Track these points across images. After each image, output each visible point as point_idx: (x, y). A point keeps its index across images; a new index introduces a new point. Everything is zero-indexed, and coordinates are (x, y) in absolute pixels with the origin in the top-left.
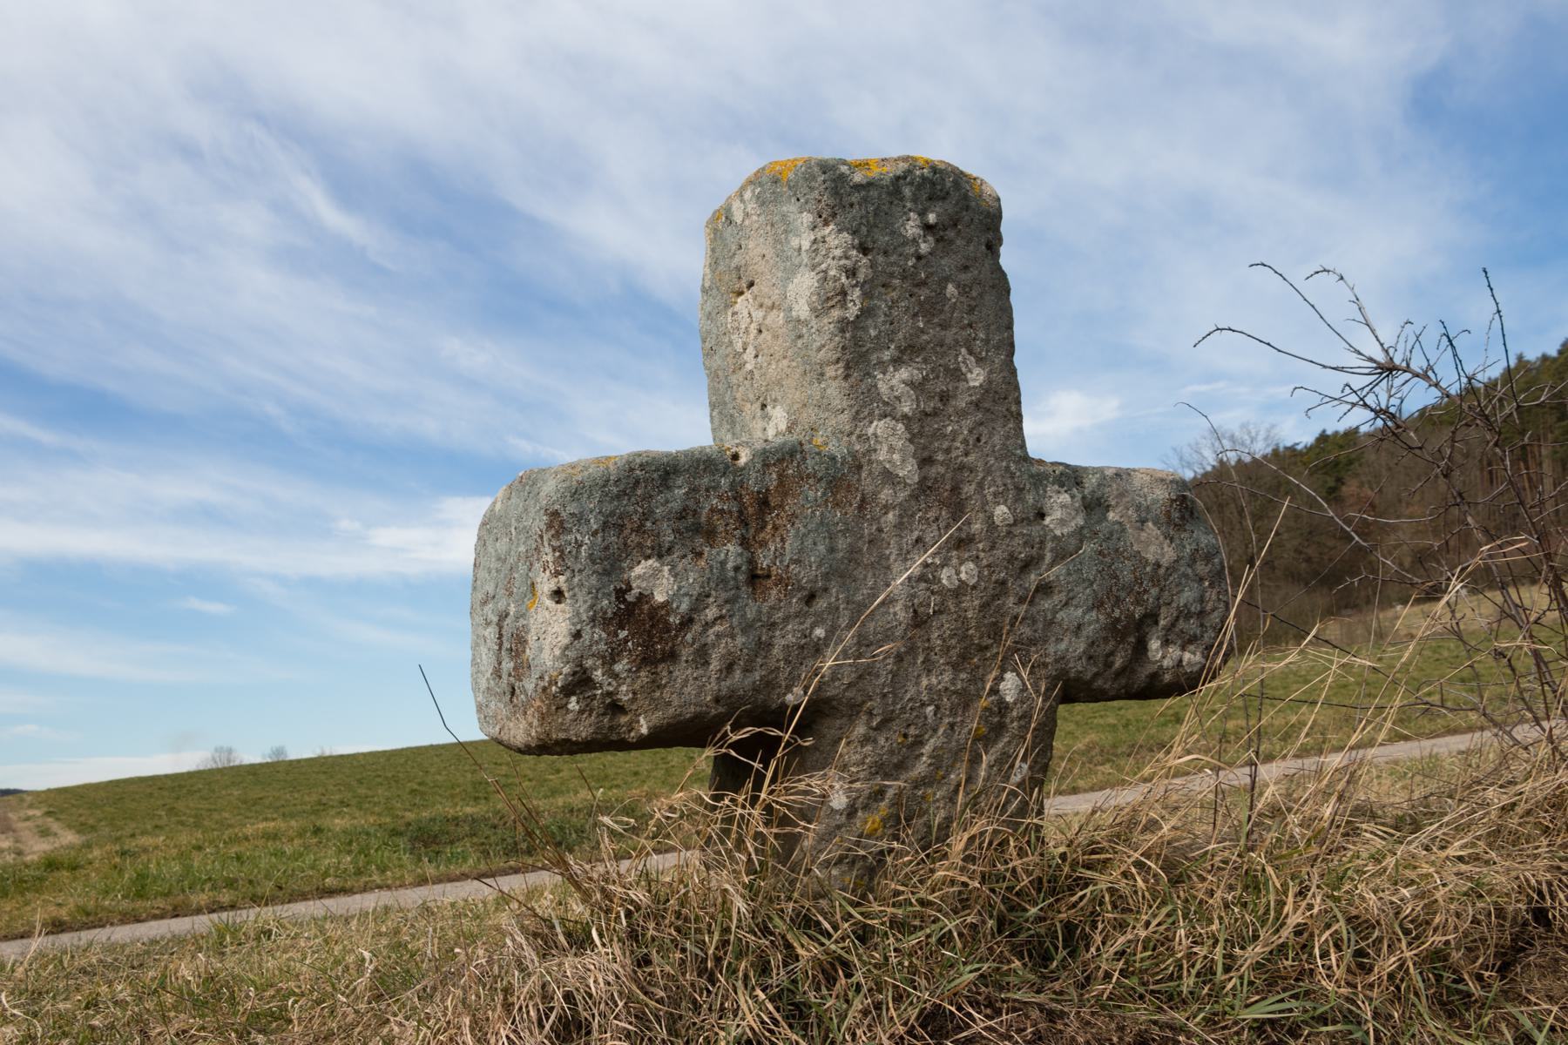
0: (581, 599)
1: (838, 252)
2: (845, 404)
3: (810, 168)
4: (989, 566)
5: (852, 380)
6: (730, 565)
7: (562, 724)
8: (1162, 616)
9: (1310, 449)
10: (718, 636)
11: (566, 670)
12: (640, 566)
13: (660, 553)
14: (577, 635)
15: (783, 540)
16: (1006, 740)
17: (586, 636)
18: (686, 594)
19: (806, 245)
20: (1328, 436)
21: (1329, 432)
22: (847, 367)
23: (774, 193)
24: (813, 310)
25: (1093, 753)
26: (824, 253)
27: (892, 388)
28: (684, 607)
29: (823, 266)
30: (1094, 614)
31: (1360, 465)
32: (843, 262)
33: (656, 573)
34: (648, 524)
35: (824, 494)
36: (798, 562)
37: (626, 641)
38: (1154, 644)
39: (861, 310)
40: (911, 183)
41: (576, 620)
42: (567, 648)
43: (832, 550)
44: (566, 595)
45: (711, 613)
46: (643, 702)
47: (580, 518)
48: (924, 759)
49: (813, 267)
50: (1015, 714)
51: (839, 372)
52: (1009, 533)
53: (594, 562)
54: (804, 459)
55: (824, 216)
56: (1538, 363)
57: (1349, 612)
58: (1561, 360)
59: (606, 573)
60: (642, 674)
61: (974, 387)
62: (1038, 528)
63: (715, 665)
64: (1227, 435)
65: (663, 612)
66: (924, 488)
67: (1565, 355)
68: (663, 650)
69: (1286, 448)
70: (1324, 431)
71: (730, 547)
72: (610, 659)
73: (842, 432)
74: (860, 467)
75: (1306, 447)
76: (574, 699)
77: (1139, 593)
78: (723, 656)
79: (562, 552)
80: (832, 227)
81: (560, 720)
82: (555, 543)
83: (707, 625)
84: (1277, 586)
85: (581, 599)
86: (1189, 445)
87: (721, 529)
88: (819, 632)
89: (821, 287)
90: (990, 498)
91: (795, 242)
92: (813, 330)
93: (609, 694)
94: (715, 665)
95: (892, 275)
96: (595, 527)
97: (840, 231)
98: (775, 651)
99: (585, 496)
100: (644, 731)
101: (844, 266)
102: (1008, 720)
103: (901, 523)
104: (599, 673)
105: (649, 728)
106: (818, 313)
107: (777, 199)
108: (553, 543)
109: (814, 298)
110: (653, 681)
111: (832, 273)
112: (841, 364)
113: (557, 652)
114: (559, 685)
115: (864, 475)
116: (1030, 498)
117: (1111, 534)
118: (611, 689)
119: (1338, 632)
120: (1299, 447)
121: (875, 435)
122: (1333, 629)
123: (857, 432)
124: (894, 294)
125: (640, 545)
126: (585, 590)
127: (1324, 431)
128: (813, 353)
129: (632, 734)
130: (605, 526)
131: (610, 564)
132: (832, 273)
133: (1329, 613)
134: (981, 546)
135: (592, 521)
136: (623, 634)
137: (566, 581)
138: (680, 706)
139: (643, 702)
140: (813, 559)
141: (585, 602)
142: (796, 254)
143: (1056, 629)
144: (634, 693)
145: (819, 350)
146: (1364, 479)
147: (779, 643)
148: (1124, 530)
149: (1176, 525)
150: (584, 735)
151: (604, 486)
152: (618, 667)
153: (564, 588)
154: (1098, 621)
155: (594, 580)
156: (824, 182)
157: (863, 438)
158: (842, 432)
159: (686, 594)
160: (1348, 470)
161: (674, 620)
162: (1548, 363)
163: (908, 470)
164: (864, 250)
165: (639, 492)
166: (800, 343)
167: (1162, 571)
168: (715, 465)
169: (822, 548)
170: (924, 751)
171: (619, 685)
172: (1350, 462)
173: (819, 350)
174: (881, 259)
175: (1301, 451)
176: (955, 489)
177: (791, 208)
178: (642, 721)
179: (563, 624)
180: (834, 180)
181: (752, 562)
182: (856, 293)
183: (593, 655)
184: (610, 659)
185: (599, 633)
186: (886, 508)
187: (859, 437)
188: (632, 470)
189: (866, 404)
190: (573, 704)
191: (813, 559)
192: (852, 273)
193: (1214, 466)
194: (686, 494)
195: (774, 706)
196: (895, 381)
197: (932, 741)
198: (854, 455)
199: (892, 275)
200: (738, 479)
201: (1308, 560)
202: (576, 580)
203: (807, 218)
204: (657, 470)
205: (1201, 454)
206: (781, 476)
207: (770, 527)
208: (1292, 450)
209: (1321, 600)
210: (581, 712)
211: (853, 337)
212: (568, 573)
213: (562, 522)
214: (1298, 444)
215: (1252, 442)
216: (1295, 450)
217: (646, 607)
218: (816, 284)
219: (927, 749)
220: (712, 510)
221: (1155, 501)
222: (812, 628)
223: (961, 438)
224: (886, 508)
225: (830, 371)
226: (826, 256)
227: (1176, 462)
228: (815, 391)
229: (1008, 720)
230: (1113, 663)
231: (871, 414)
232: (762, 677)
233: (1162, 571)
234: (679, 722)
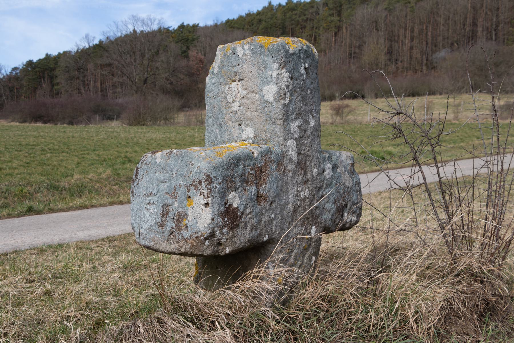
0: (215, 207)
1: (285, 80)
2: (282, 134)
3: (279, 46)
4: (311, 190)
5: (284, 126)
6: (253, 193)
7: (202, 249)
8: (348, 205)
9: (175, 31)
10: (250, 219)
11: (209, 232)
12: (231, 195)
13: (236, 189)
14: (213, 219)
15: (266, 184)
16: (311, 249)
17: (216, 220)
18: (242, 204)
19: (275, 75)
20: (184, 26)
21: (185, 24)
22: (284, 121)
23: (260, 51)
24: (275, 99)
25: (110, 180)
26: (281, 79)
27: (294, 128)
28: (242, 209)
29: (280, 84)
30: (334, 205)
31: (198, 42)
32: (287, 83)
33: (234, 198)
34: (233, 179)
35: (276, 167)
36: (269, 191)
37: (227, 221)
38: (346, 214)
39: (289, 101)
40: (302, 52)
41: (213, 214)
42: (210, 224)
43: (277, 187)
44: (210, 205)
45: (248, 211)
46: (229, 242)
47: (216, 177)
48: (293, 257)
49: (277, 84)
50: (314, 240)
51: (281, 123)
52: (316, 178)
53: (220, 194)
54: (271, 154)
55: (282, 65)
56: (277, 7)
57: (187, 109)
58: (286, 7)
59: (222, 197)
60: (230, 233)
61: (312, 127)
62: (323, 176)
63: (249, 229)
64: (141, 19)
65: (236, 211)
66: (298, 163)
67: (288, 5)
68: (236, 224)
69: (164, 28)
70: (183, 23)
71: (253, 187)
72: (221, 228)
73: (279, 144)
74: (284, 157)
75: (174, 29)
76: (207, 241)
77: (344, 197)
78: (251, 226)
79: (211, 190)
80: (284, 70)
81: (201, 248)
82: (208, 186)
83: (247, 215)
84: (157, 95)
85: (215, 207)
86: (122, 22)
87: (250, 180)
88: (273, 216)
89: (279, 91)
90: (313, 166)
91: (270, 73)
92: (274, 106)
93: (219, 239)
94: (249, 229)
95: (297, 88)
96: (220, 181)
97: (287, 72)
98: (262, 223)
99: (217, 169)
100: (227, 252)
101: (286, 85)
102: (312, 242)
103: (293, 176)
104: (218, 232)
105: (229, 251)
106: (277, 101)
107: (262, 53)
108: (208, 186)
109: (276, 95)
110: (233, 235)
111: (283, 87)
112: (282, 120)
113: (206, 226)
114: (205, 236)
115: (285, 159)
116: (322, 166)
117: (338, 177)
118: (220, 238)
119: (184, 118)
120: (171, 29)
121: (289, 145)
122: (181, 117)
123: (284, 144)
124: (296, 94)
125: (231, 187)
126: (217, 204)
127: (183, 23)
128: (272, 115)
129: (223, 253)
130: (223, 180)
131: (223, 194)
132: (283, 87)
133: (181, 108)
134: (310, 183)
135: (219, 179)
136: (226, 219)
137: (211, 200)
138: (239, 244)
139: (229, 242)
140: (273, 190)
141: (216, 208)
142: (269, 77)
143: (324, 211)
144: (227, 239)
145: (275, 114)
146: (198, 48)
147: (264, 220)
148: (341, 176)
149: (484, 234)
150: (209, 253)
151: (223, 166)
152: (224, 231)
153: (210, 202)
154: (334, 208)
155: (219, 200)
156: (283, 52)
157: (286, 146)
158: (279, 144)
159: (242, 204)
160: (192, 43)
161: (239, 213)
162: (281, 8)
163: (295, 158)
164: (291, 78)
165: (231, 168)
166: (266, 109)
167: (349, 189)
168: (249, 157)
169: (275, 186)
170: (292, 254)
171: (223, 237)
172: (193, 40)
173: (275, 114)
174: (295, 82)
175: (171, 31)
176: (305, 164)
177: (269, 60)
178: (227, 248)
179: (209, 216)
180: (286, 52)
181: (258, 192)
182: (288, 95)
183: (218, 227)
184: (221, 228)
185: (220, 219)
186: (290, 171)
187: (285, 146)
188: (230, 160)
189: (287, 134)
190: (207, 243)
191: (273, 190)
192: (288, 87)
193: (131, 32)
194: (243, 168)
195: (260, 242)
196: (294, 125)
197: (295, 251)
198: (283, 152)
199: (297, 88)
200: (255, 162)
201: (171, 83)
202: (214, 200)
203: (276, 65)
204: (236, 160)
205: (127, 26)
206: (265, 160)
207: (262, 179)
208: (167, 30)
209: (178, 103)
210: (209, 245)
211: (286, 110)
212: (212, 198)
213: (211, 179)
214: (170, 27)
215: (152, 25)
216: (169, 30)
217: (231, 209)
218: (277, 90)
219: (294, 254)
220: (249, 174)
221: (348, 164)
222: (271, 214)
223: (308, 145)
224: (290, 171)
225: (278, 122)
226: (282, 80)
227: (115, 29)
228: (271, 127)
229: (312, 242)
230: (336, 221)
231: (288, 138)
232: (259, 232)
233: (349, 189)
234: (239, 249)
